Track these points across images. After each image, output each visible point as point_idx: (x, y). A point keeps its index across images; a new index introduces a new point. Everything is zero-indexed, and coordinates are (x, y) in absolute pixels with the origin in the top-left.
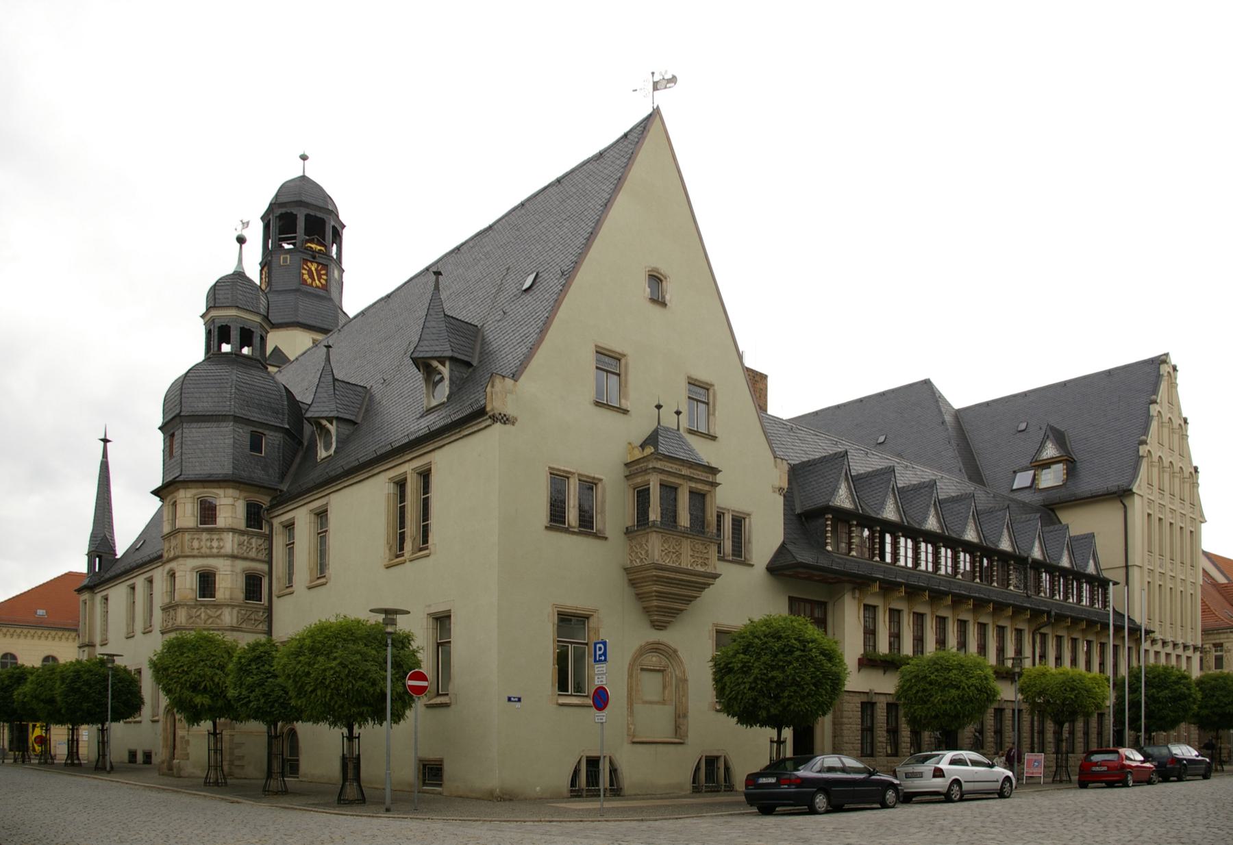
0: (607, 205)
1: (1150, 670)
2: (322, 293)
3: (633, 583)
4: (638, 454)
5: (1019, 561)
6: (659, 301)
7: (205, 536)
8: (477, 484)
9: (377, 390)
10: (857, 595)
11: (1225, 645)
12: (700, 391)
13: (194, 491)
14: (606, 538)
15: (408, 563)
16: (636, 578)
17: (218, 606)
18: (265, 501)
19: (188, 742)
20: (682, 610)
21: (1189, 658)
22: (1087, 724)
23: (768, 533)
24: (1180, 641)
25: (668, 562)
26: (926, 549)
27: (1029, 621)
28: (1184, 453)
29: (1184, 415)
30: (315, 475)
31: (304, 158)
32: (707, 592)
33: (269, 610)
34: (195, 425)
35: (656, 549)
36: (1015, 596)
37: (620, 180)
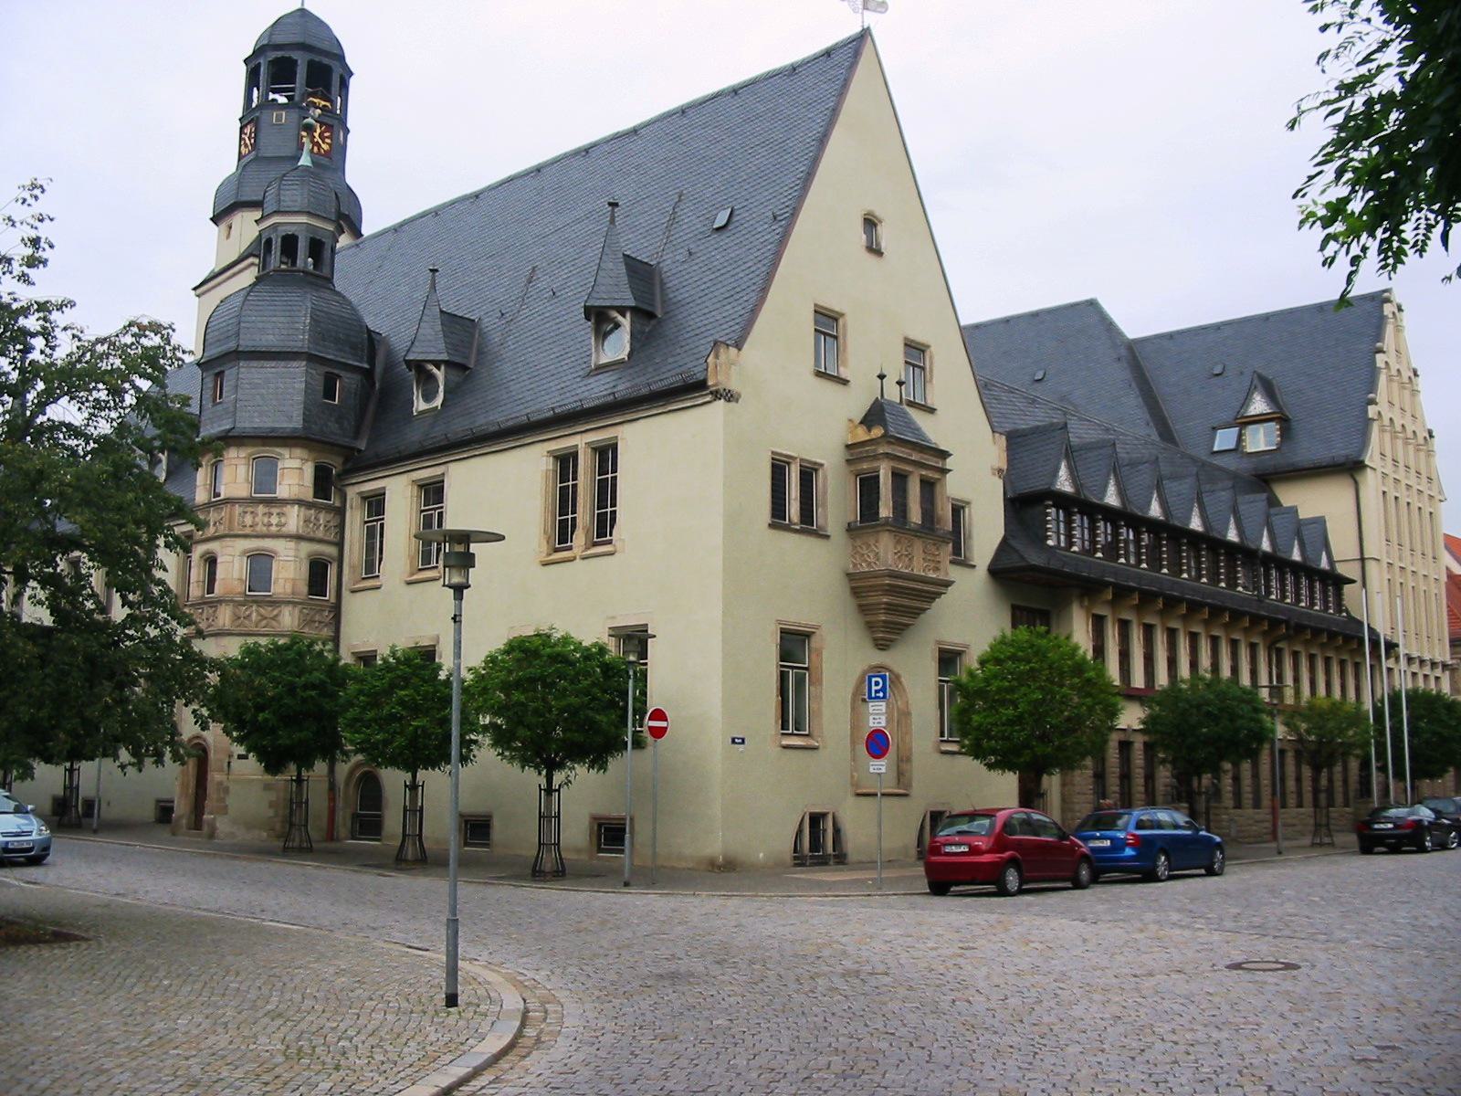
0: (823, 140)
1: (1414, 696)
3: (855, 592)
4: (862, 435)
5: (1209, 543)
6: (874, 250)
7: (261, 509)
8: (681, 472)
9: (490, 323)
10: (1086, 603)
12: (915, 351)
13: (250, 450)
14: (827, 537)
15: (578, 560)
16: (860, 587)
17: (275, 603)
18: (336, 464)
19: (227, 790)
20: (907, 625)
21: (1437, 678)
22: (1255, 766)
23: (987, 529)
25: (901, 567)
26: (1104, 531)
27: (1264, 634)
29: (1414, 366)
33: (337, 609)
34: (255, 363)
35: (885, 553)
36: (1245, 599)
37: (835, 112)
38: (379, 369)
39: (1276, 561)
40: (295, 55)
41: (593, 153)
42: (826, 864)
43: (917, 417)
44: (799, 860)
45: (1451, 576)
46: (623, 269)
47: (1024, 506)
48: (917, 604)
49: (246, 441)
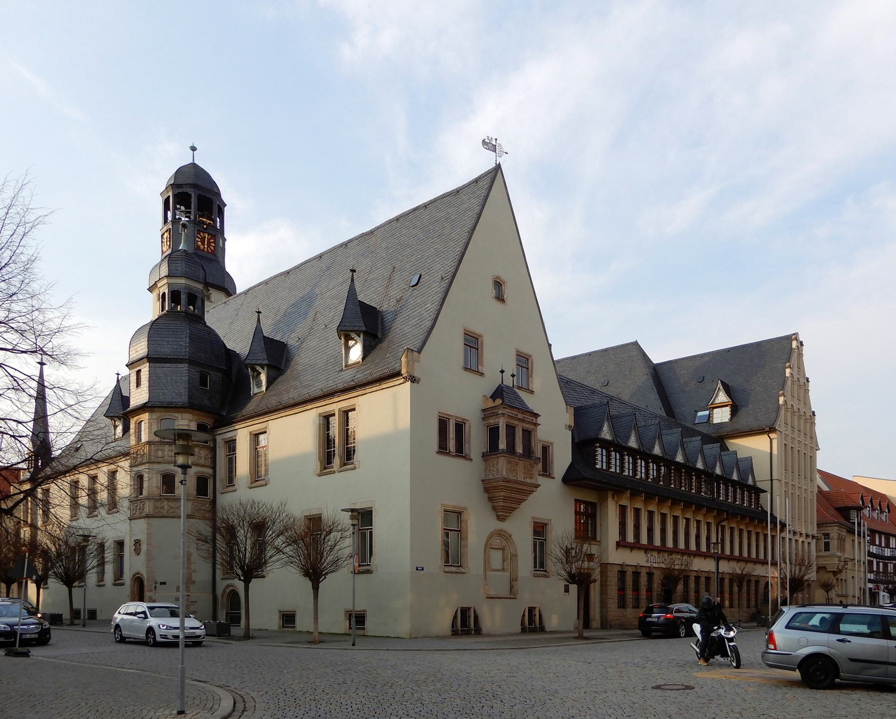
2: (211, 256)
3: (486, 490)
4: (491, 404)
5: (688, 469)
6: (500, 298)
11: (831, 535)
12: (524, 361)
13: (158, 414)
16: (489, 488)
21: (809, 543)
23: (562, 458)
24: (804, 532)
25: (511, 477)
28: (806, 402)
30: (250, 407)
31: (193, 149)
32: (532, 497)
35: (502, 467)
38: (234, 371)
39: (725, 480)
40: (190, 191)
41: (350, 245)
42: (470, 634)
43: (521, 394)
44: (455, 633)
45: (820, 491)
46: (358, 309)
47: (583, 446)
48: (519, 496)
49: (156, 409)
